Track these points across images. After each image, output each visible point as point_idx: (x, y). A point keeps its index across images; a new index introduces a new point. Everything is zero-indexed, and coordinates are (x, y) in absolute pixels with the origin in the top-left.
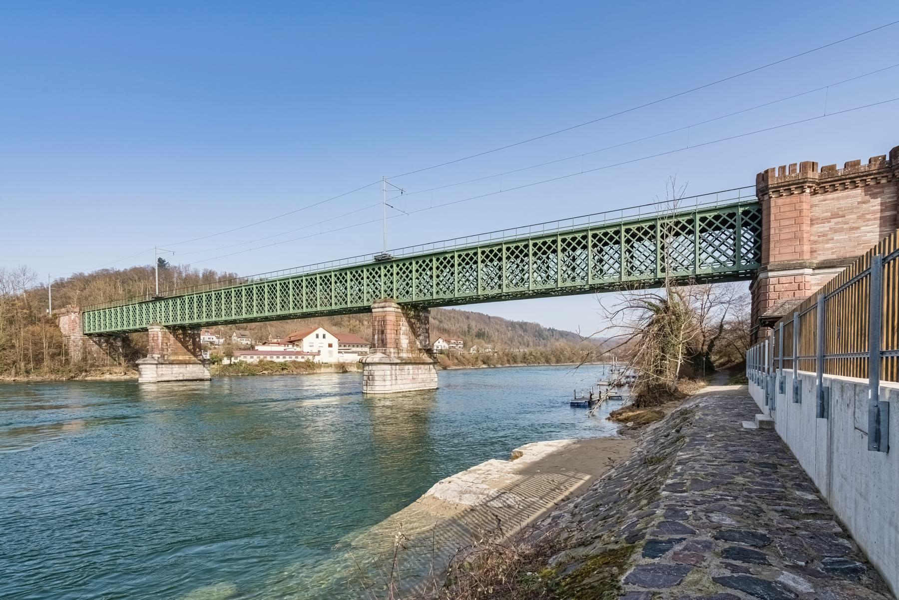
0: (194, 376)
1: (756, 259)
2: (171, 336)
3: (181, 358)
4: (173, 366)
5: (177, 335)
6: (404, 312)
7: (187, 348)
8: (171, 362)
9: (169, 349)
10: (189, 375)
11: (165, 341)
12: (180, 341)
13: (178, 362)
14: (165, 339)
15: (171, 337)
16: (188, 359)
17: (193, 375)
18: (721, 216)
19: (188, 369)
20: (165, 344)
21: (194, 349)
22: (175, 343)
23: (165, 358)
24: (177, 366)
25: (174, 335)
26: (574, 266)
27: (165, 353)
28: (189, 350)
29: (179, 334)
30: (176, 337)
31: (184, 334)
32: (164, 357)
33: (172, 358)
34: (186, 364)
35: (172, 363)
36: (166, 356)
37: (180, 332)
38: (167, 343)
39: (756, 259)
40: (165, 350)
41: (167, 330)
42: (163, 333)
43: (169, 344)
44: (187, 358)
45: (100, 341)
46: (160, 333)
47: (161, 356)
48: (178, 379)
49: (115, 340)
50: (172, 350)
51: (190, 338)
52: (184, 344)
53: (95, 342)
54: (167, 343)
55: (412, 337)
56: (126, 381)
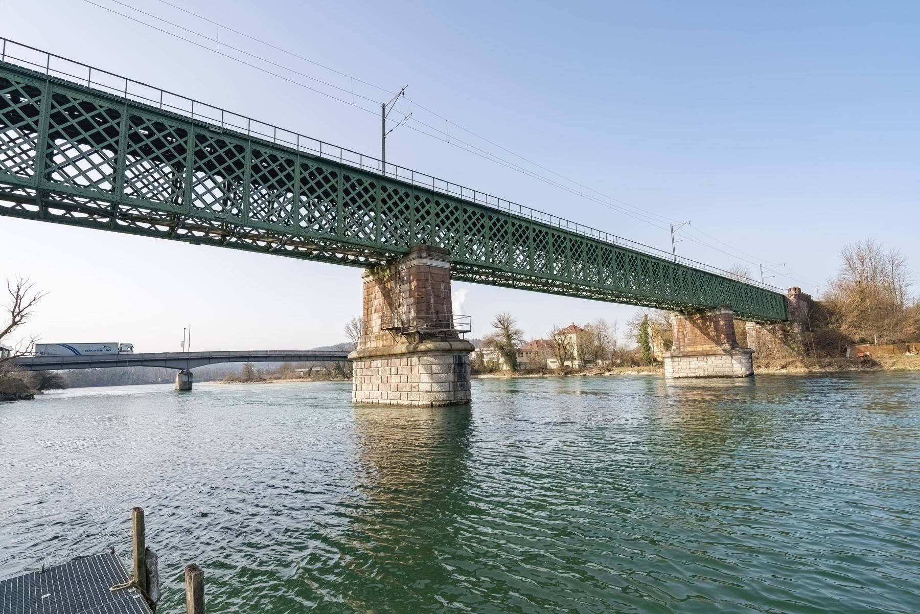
0: (720, 371)
1: (309, 195)
2: (687, 322)
3: (699, 348)
4: (691, 359)
5: (694, 322)
6: (377, 277)
7: (707, 335)
8: (685, 354)
9: (686, 339)
10: (711, 370)
11: (681, 330)
12: (700, 328)
13: (694, 354)
14: (680, 327)
15: (688, 323)
16: (708, 349)
17: (717, 370)
18: (227, 145)
19: (709, 362)
20: (681, 334)
21: (718, 336)
22: (692, 332)
23: (682, 350)
24: (695, 359)
25: (690, 321)
26: (454, 225)
27: (681, 343)
28: (710, 338)
29: (697, 319)
30: (693, 322)
31: (703, 318)
32: (680, 349)
33: (689, 349)
34: (707, 355)
35: (686, 355)
36: (682, 348)
37: (698, 316)
38: (683, 332)
39: (309, 195)
40: (681, 340)
41: (682, 317)
42: (678, 320)
43: (685, 332)
44: (707, 347)
45: (774, 329)
46: (674, 321)
47: (677, 348)
48: (697, 374)
49: (790, 325)
50: (689, 340)
51: (710, 322)
52: (704, 331)
53: (768, 330)
54: (683, 332)
55: (387, 312)
56: (783, 375)
